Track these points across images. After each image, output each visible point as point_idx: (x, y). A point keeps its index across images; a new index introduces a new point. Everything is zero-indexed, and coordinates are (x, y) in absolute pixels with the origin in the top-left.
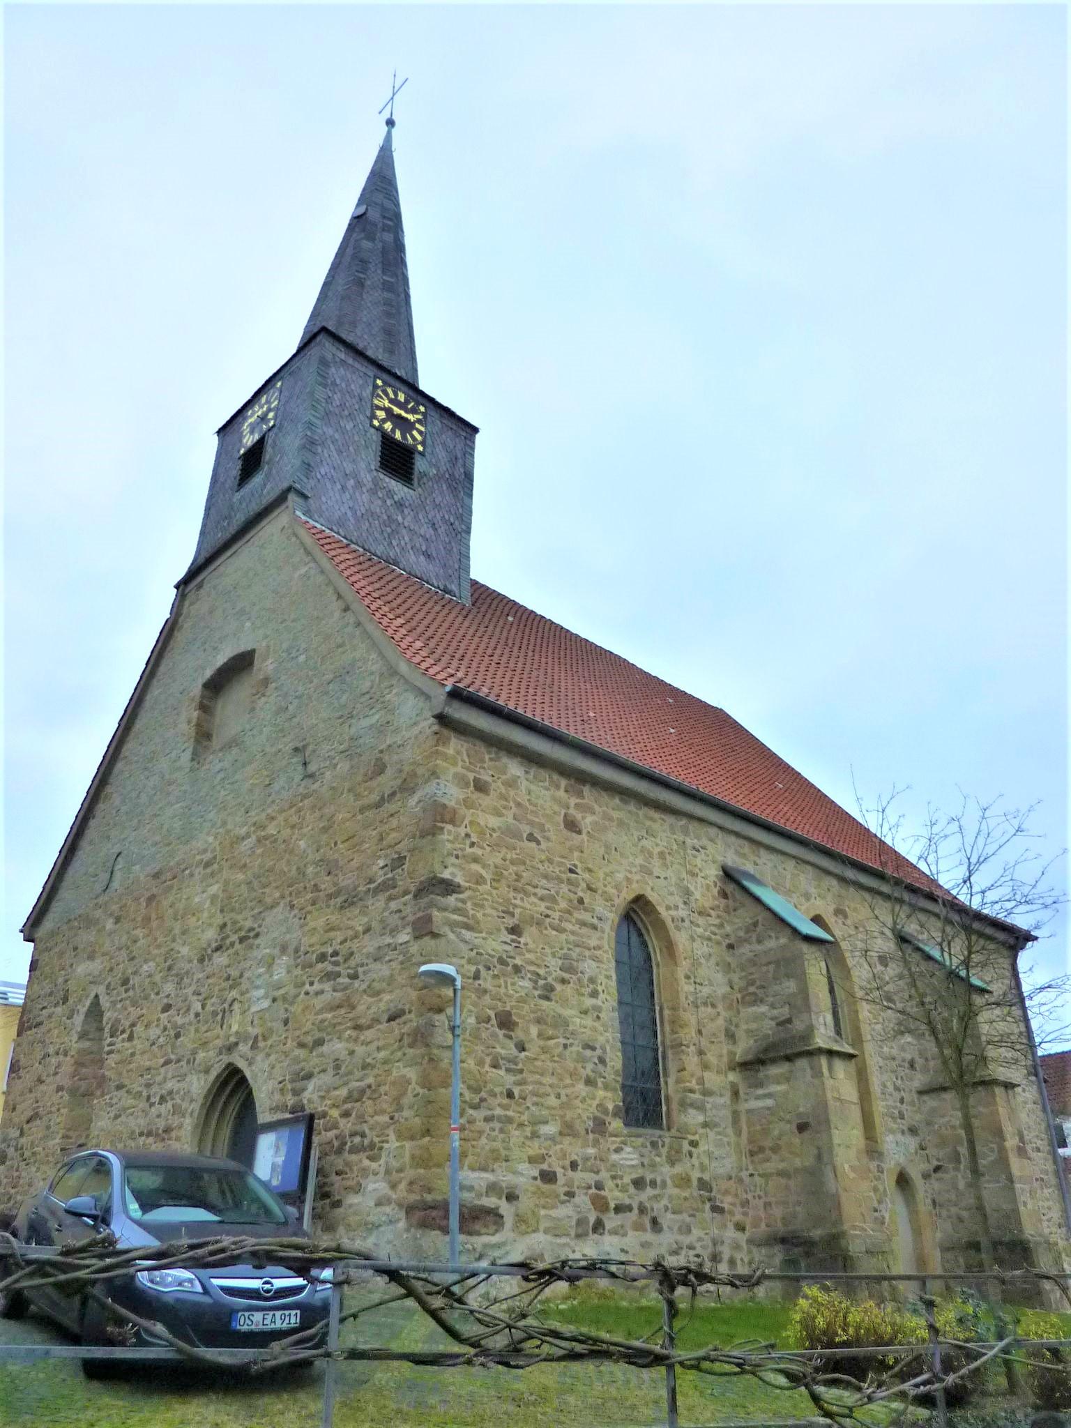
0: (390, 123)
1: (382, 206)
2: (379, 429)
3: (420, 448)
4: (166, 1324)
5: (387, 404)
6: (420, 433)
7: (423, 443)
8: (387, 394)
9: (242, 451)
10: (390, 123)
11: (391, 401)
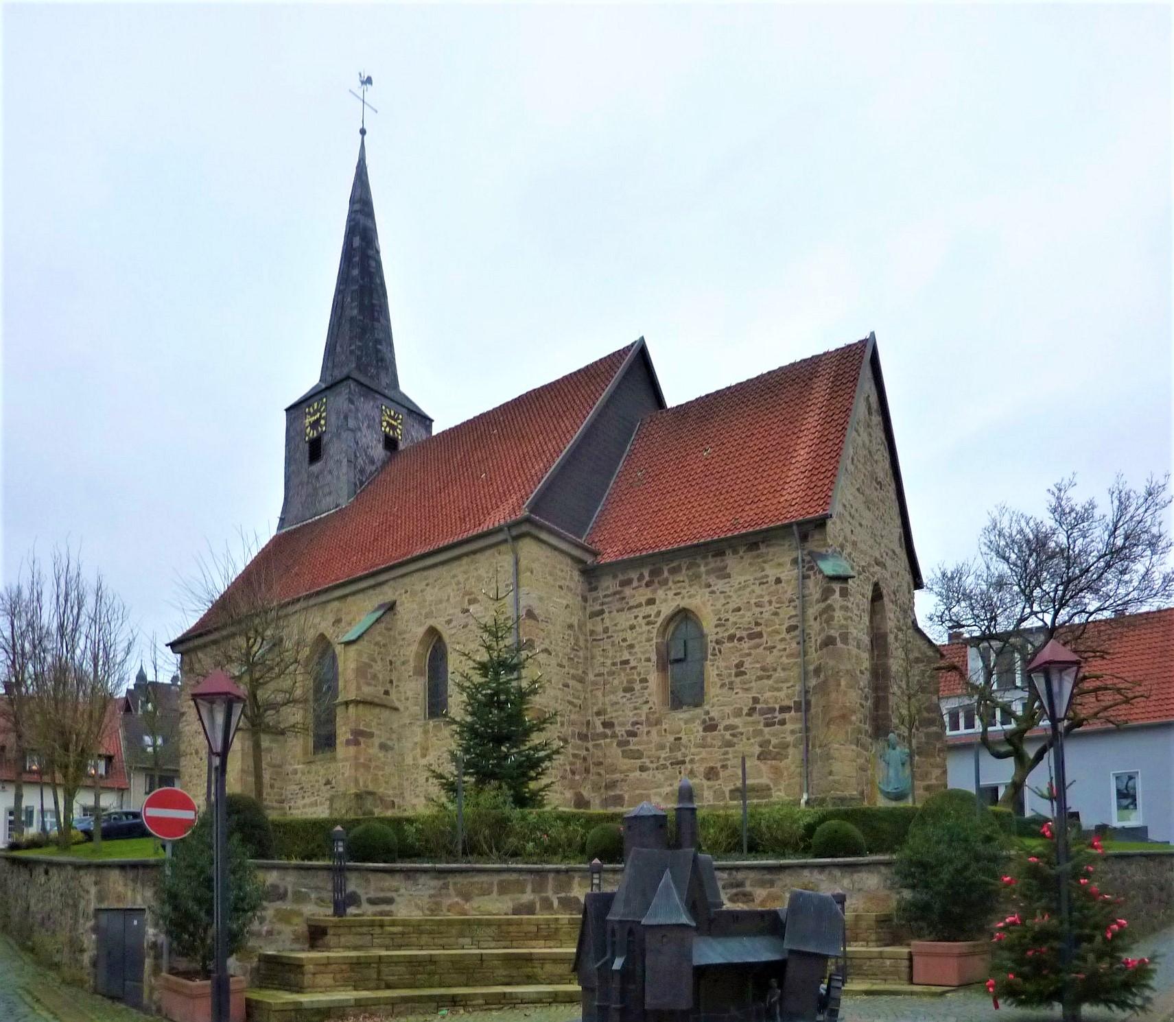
0: (363, 132)
10: (363, 132)
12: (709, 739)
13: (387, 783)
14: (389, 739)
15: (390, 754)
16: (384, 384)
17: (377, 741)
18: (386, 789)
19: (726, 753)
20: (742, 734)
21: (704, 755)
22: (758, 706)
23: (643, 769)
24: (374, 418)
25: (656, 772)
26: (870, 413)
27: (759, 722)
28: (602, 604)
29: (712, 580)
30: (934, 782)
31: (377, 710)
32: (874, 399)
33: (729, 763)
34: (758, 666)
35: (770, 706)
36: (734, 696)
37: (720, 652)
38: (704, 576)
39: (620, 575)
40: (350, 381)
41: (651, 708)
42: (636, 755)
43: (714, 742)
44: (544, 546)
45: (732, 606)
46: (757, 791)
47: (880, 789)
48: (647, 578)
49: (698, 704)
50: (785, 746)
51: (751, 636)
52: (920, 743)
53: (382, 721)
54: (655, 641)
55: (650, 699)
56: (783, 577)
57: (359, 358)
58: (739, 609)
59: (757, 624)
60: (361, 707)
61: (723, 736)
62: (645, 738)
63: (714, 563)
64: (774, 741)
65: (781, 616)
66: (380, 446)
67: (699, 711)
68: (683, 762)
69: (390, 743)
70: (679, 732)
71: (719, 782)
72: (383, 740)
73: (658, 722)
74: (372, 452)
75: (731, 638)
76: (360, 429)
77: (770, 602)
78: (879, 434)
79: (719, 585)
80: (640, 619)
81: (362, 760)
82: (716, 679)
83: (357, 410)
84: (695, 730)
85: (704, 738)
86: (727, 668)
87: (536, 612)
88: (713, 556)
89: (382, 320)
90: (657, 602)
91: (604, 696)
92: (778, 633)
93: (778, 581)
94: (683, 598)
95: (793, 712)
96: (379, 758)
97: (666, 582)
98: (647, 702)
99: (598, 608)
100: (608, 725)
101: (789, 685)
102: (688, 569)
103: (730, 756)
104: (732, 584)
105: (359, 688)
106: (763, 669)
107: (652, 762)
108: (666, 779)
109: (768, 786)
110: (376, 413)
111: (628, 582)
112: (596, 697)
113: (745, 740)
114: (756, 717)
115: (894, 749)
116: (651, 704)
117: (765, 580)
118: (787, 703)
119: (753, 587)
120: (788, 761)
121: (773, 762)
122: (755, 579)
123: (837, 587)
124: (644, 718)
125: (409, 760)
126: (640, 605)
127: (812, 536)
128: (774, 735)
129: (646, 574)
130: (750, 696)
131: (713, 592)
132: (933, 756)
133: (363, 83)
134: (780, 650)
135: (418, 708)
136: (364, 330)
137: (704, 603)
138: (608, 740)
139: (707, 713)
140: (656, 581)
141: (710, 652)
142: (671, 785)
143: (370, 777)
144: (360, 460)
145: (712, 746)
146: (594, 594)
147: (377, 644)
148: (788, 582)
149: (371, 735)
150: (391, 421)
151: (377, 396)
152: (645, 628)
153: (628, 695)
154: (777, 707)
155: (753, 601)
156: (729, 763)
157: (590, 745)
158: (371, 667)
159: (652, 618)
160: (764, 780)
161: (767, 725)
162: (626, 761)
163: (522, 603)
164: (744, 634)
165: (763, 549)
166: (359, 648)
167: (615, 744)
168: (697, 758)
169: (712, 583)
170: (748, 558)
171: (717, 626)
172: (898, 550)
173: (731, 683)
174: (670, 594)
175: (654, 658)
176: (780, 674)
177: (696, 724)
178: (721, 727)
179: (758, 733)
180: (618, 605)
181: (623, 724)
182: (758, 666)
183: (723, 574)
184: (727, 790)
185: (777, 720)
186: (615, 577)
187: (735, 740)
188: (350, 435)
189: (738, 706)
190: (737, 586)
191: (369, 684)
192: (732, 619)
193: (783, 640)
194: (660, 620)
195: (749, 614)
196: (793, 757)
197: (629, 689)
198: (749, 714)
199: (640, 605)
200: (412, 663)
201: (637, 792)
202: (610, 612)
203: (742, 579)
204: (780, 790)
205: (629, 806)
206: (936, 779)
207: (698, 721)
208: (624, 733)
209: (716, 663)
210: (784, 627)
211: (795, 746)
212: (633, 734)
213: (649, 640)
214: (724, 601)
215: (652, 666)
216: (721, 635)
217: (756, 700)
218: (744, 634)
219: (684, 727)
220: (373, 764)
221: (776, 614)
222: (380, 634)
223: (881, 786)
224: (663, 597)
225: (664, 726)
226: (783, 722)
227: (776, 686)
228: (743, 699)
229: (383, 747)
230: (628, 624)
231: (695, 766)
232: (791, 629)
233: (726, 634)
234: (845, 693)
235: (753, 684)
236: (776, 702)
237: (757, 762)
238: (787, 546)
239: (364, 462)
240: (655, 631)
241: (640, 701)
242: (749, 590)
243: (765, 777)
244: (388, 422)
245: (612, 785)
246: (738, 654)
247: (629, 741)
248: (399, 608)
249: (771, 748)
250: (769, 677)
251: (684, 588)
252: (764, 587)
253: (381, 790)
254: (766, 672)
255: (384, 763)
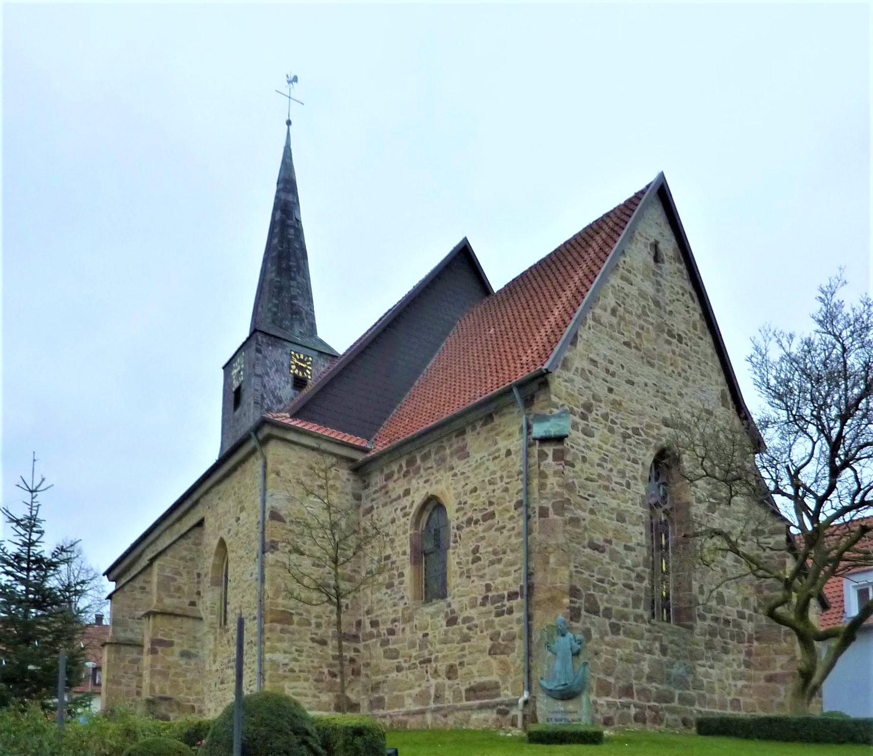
0: (289, 123)
1: (383, 673)
2: (294, 374)
3: (309, 377)
4: (33, 664)
5: (296, 361)
6: (310, 370)
7: (311, 375)
8: (296, 357)
9: (234, 389)
10: (289, 123)
11: (297, 360)
12: (450, 635)
13: (189, 689)
14: (193, 647)
15: (193, 662)
16: (297, 333)
17: (177, 649)
18: (186, 694)
19: (463, 649)
20: (476, 626)
21: (445, 652)
22: (490, 594)
23: (399, 669)
24: (283, 364)
25: (408, 671)
26: (657, 258)
27: (490, 612)
28: (373, 500)
29: (455, 462)
30: (778, 671)
31: (179, 620)
32: (668, 246)
33: (465, 660)
34: (490, 549)
35: (500, 593)
36: (471, 585)
37: (460, 537)
38: (448, 459)
39: (385, 469)
40: (258, 333)
41: (406, 604)
42: (394, 654)
43: (454, 637)
44: (296, 448)
45: (469, 487)
46: (488, 690)
47: (542, 686)
48: (405, 469)
49: (444, 596)
50: (512, 638)
51: (486, 517)
52: (759, 627)
53: (184, 630)
54: (409, 532)
55: (405, 595)
56: (513, 449)
57: (275, 313)
58: (475, 490)
59: (491, 503)
60: (159, 618)
61: (461, 629)
62: (401, 636)
63: (456, 443)
64: (503, 632)
65: (511, 492)
66: (289, 386)
67: (442, 604)
68: (429, 661)
69: (193, 651)
70: (426, 628)
71: (457, 681)
72: (185, 648)
73: (410, 619)
74: (279, 393)
75: (469, 522)
76: (267, 374)
77: (502, 478)
78: (677, 281)
79: (460, 466)
80: (398, 511)
81: (159, 667)
82: (457, 569)
83: (265, 357)
84: (439, 625)
85: (446, 633)
86: (466, 555)
87: (283, 513)
88: (457, 436)
89: (299, 279)
90: (412, 492)
91: (372, 594)
92: (508, 511)
93: (509, 453)
94: (431, 485)
95: (519, 599)
96: (181, 666)
97: (417, 471)
98: (402, 598)
99: (369, 505)
100: (374, 624)
101: (516, 567)
102: (436, 453)
103: (466, 652)
104: (471, 463)
105: (160, 600)
106: (495, 553)
107: (405, 661)
108: (416, 680)
109: (497, 683)
110: (285, 358)
111: (389, 477)
112: (366, 595)
113: (479, 633)
114: (489, 607)
115: (563, 635)
116: (406, 600)
117: (497, 454)
118: (516, 588)
119: (487, 463)
120: (514, 655)
121: (502, 657)
122: (490, 455)
123: (549, 449)
124: (400, 615)
125: (207, 668)
126: (399, 498)
127: (538, 397)
128: (503, 626)
129: (404, 465)
130: (484, 583)
131: (455, 475)
132: (778, 642)
133: (289, 82)
134: (509, 530)
135: (213, 616)
136: (280, 289)
137: (448, 488)
138: (374, 640)
139: (449, 605)
140: (411, 471)
141: (452, 538)
142: (420, 686)
143: (168, 683)
144: (267, 401)
145: (452, 641)
146: (367, 491)
147: (182, 558)
148: (516, 452)
149: (171, 644)
150: (299, 363)
151: (286, 343)
152: (403, 520)
153: (389, 591)
154: (506, 593)
155: (486, 480)
156: (465, 660)
157: (360, 646)
158: (175, 580)
159: (407, 510)
160: (494, 678)
161: (499, 614)
162: (387, 661)
163: (268, 505)
164: (479, 516)
165: (497, 420)
166: (162, 563)
167: (379, 644)
168: (440, 655)
169: (455, 465)
170: (484, 432)
171: (457, 511)
172: (720, 411)
173: (468, 571)
174: (421, 481)
175: (408, 551)
176: (509, 557)
177: (440, 618)
178: (460, 620)
179: (490, 624)
180: (383, 500)
181: (384, 622)
182: (490, 549)
183: (463, 454)
184: (463, 689)
185: (505, 608)
186: (382, 471)
187: (471, 633)
188: (258, 380)
189: (474, 595)
190: (474, 465)
191: (172, 596)
192: (470, 501)
193: (512, 518)
194: (413, 511)
195: (484, 494)
196: (520, 645)
197: (390, 586)
198: (483, 604)
199: (399, 498)
200: (210, 575)
201: (395, 693)
202: (377, 508)
203: (478, 456)
204: (507, 688)
205: (389, 708)
206: (782, 667)
207: (442, 615)
208: (385, 632)
209: (457, 550)
210: (513, 504)
211: (520, 638)
212: (392, 632)
213: (405, 533)
214: (463, 483)
215: (407, 558)
216: (461, 520)
217: (488, 588)
218: (479, 516)
219: (430, 621)
220: (173, 671)
221: (506, 490)
222: (186, 549)
223: (544, 683)
224: (416, 486)
225: (416, 622)
226: (510, 611)
227: (505, 570)
228: (477, 588)
229: (185, 654)
230: (390, 518)
231: (438, 665)
232: (519, 504)
233: (465, 518)
234: (555, 571)
235: (486, 571)
236: (505, 589)
237: (488, 658)
238: (516, 413)
239: (272, 402)
240: (409, 522)
241: (398, 596)
242: (484, 467)
243: (495, 674)
244: (297, 365)
245: (376, 687)
246: (474, 539)
247: (388, 641)
248: (206, 524)
249: (500, 641)
250: (499, 561)
251: (433, 474)
252: (496, 461)
253: (182, 695)
254: (497, 557)
255: (187, 670)
